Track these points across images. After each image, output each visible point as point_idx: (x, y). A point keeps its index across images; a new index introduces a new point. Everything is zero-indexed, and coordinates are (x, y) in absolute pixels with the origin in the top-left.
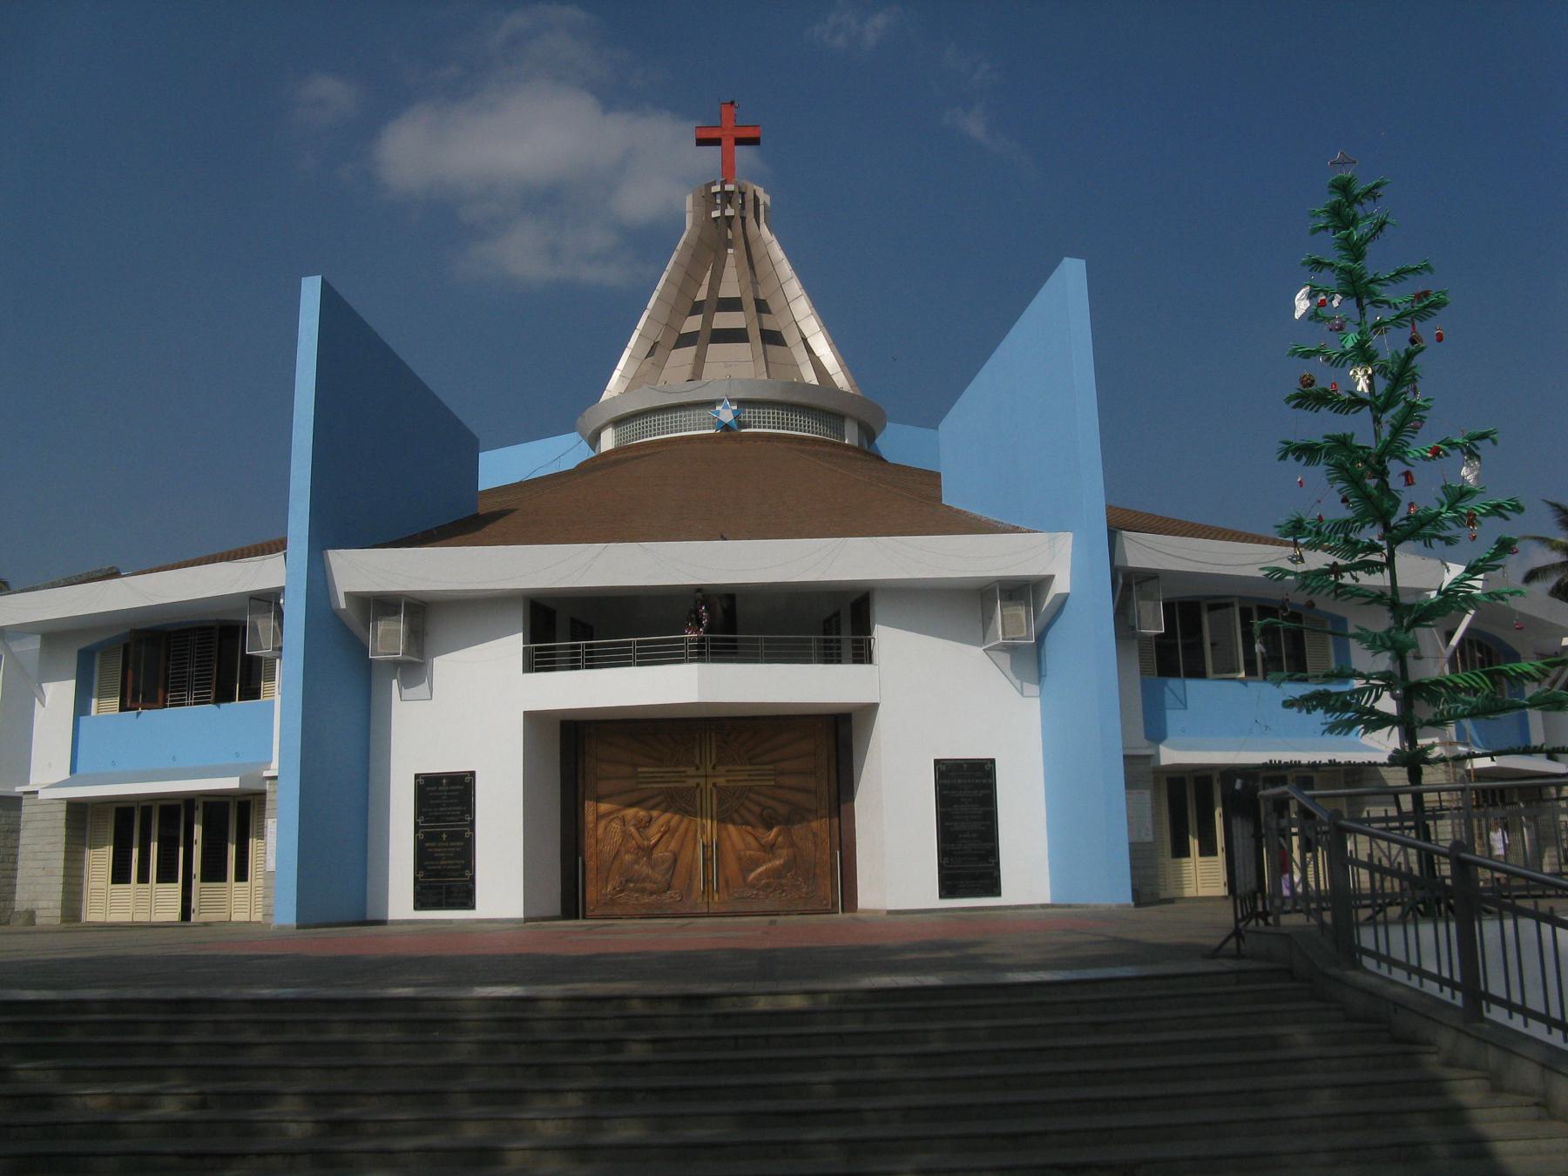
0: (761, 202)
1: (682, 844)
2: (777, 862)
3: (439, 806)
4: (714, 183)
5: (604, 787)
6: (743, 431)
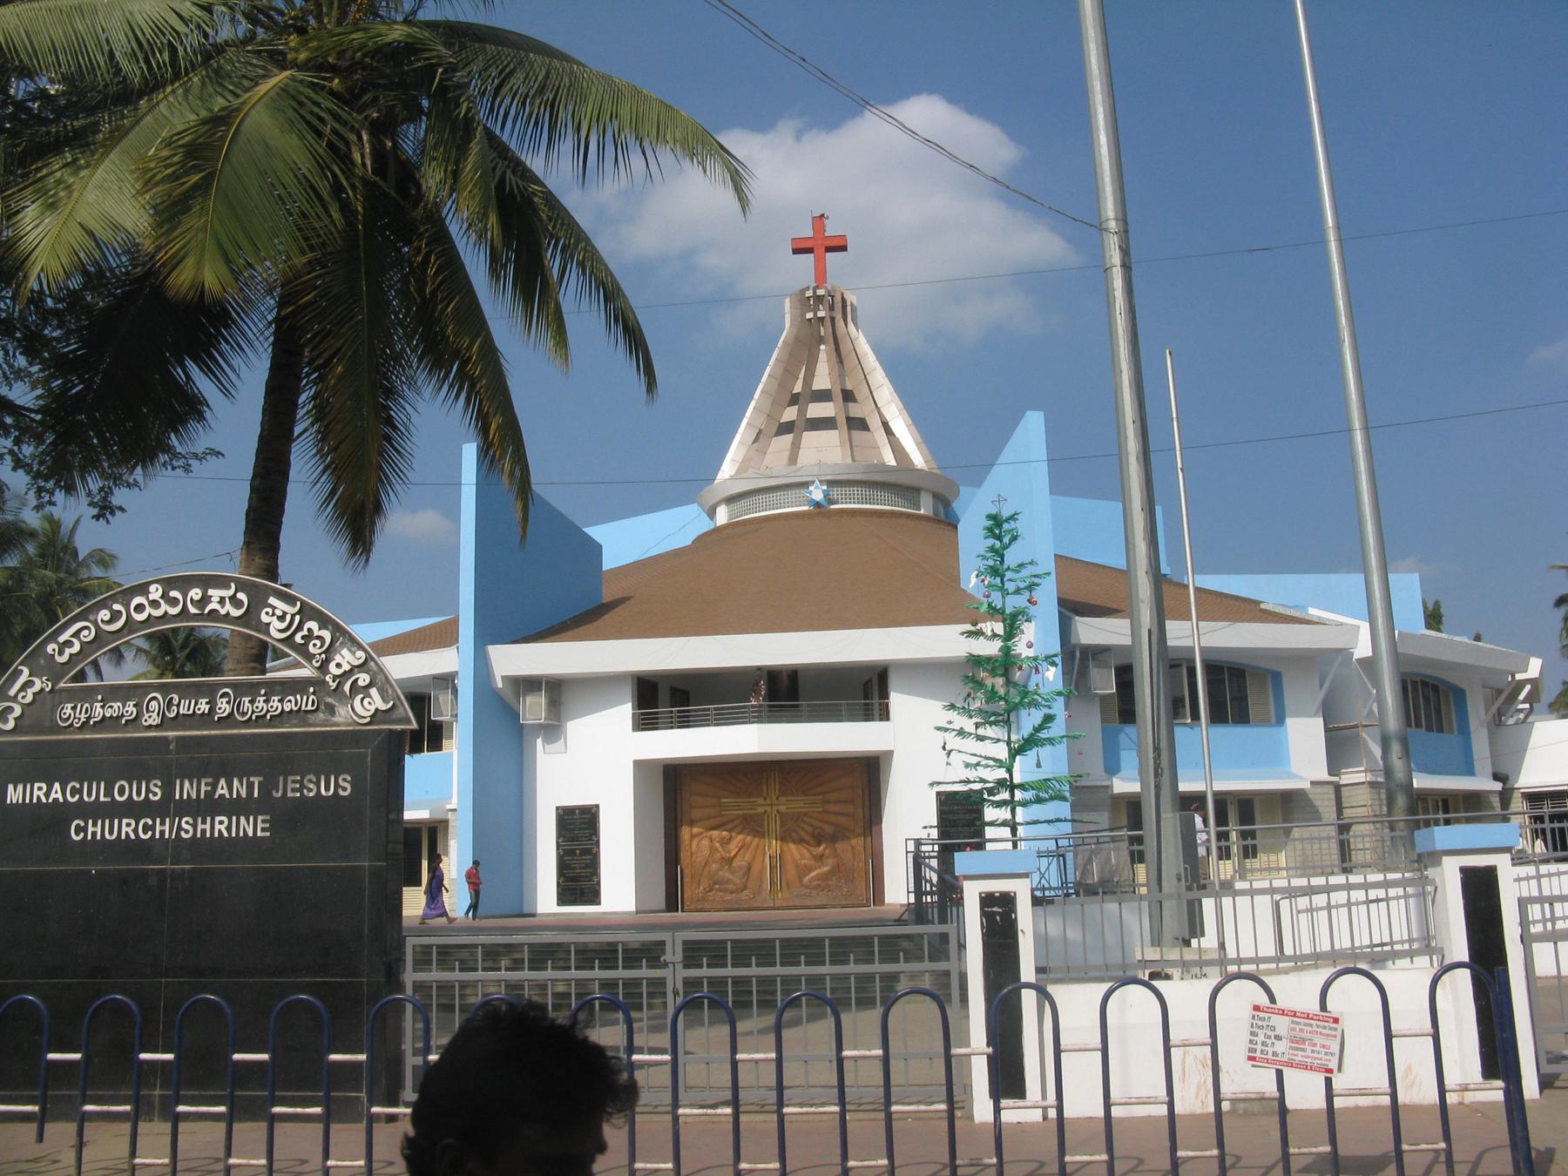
0: (848, 303)
1: (754, 857)
2: (825, 869)
3: (574, 830)
4: (808, 289)
5: (696, 814)
6: (832, 507)
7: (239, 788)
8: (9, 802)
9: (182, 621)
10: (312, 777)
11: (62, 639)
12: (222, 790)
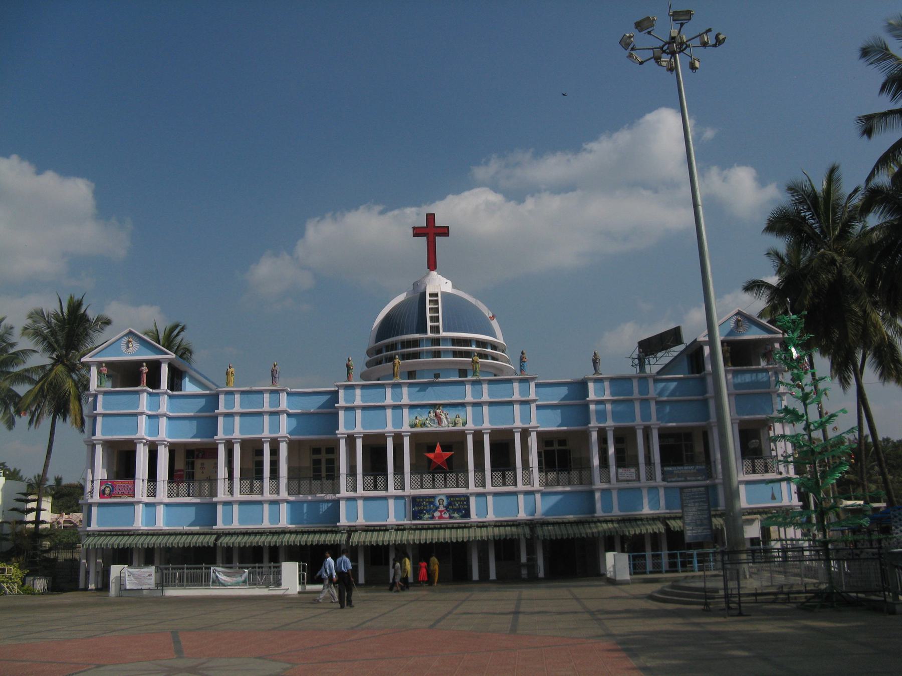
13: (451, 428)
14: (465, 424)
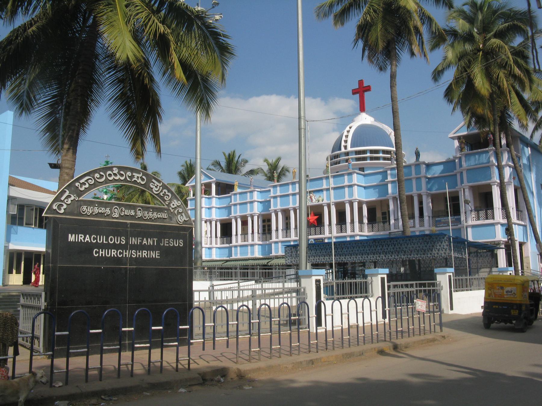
7: (150, 242)
8: (69, 240)
9: (124, 182)
10: (172, 240)
11: (82, 181)
12: (145, 242)
13: (317, 203)
14: (323, 200)
